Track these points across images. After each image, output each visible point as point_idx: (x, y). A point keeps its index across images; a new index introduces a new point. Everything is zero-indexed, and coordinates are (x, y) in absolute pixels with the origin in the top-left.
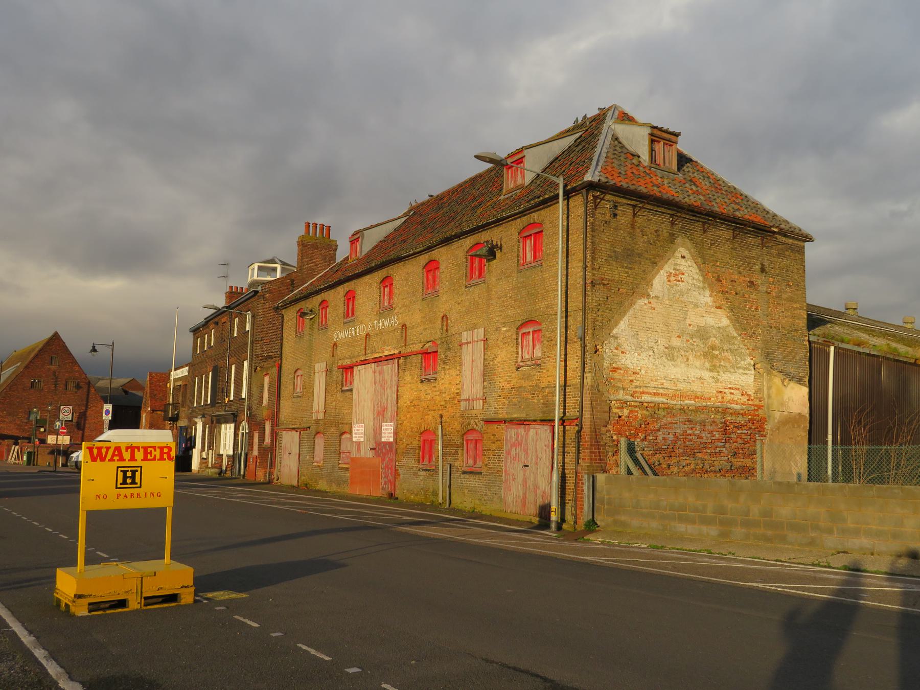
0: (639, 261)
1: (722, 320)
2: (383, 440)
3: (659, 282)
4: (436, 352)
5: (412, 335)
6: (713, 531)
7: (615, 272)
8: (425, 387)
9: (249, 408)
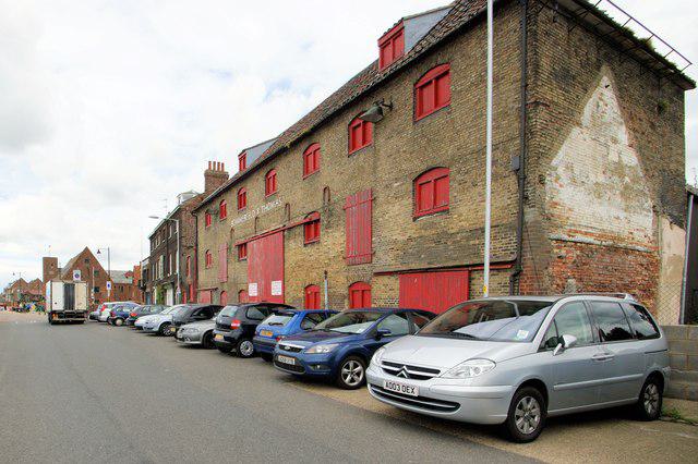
0: (575, 82)
1: (631, 158)
2: (373, 306)
3: (588, 109)
4: (318, 220)
5: (295, 210)
6: (161, 277)
7: (549, 92)
8: (310, 250)
9: (181, 279)
